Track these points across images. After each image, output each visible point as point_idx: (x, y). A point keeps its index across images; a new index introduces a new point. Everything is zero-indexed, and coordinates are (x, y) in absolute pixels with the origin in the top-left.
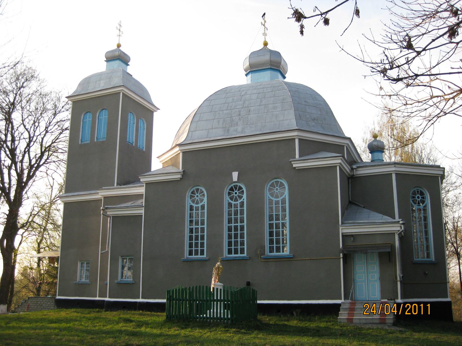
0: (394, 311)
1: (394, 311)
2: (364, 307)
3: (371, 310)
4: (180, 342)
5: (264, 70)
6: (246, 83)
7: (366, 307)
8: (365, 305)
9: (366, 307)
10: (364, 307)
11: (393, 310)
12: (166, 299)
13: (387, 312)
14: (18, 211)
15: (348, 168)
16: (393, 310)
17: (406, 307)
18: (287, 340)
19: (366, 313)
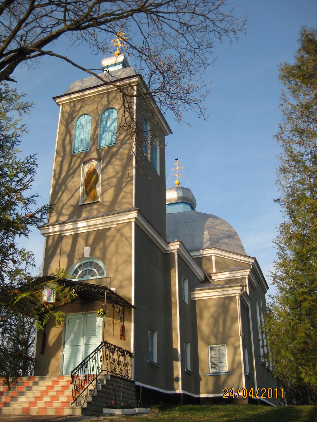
0: (251, 395)
1: (251, 395)
2: (224, 391)
3: (249, 394)
4: (89, 411)
5: (176, 204)
6: (182, 211)
7: (226, 391)
8: (224, 390)
9: (226, 391)
10: (224, 391)
11: (250, 394)
12: (135, 380)
13: (270, 396)
14: (53, 328)
15: (202, 274)
16: (250, 394)
17: (262, 391)
18: (199, 416)
19: (225, 396)
